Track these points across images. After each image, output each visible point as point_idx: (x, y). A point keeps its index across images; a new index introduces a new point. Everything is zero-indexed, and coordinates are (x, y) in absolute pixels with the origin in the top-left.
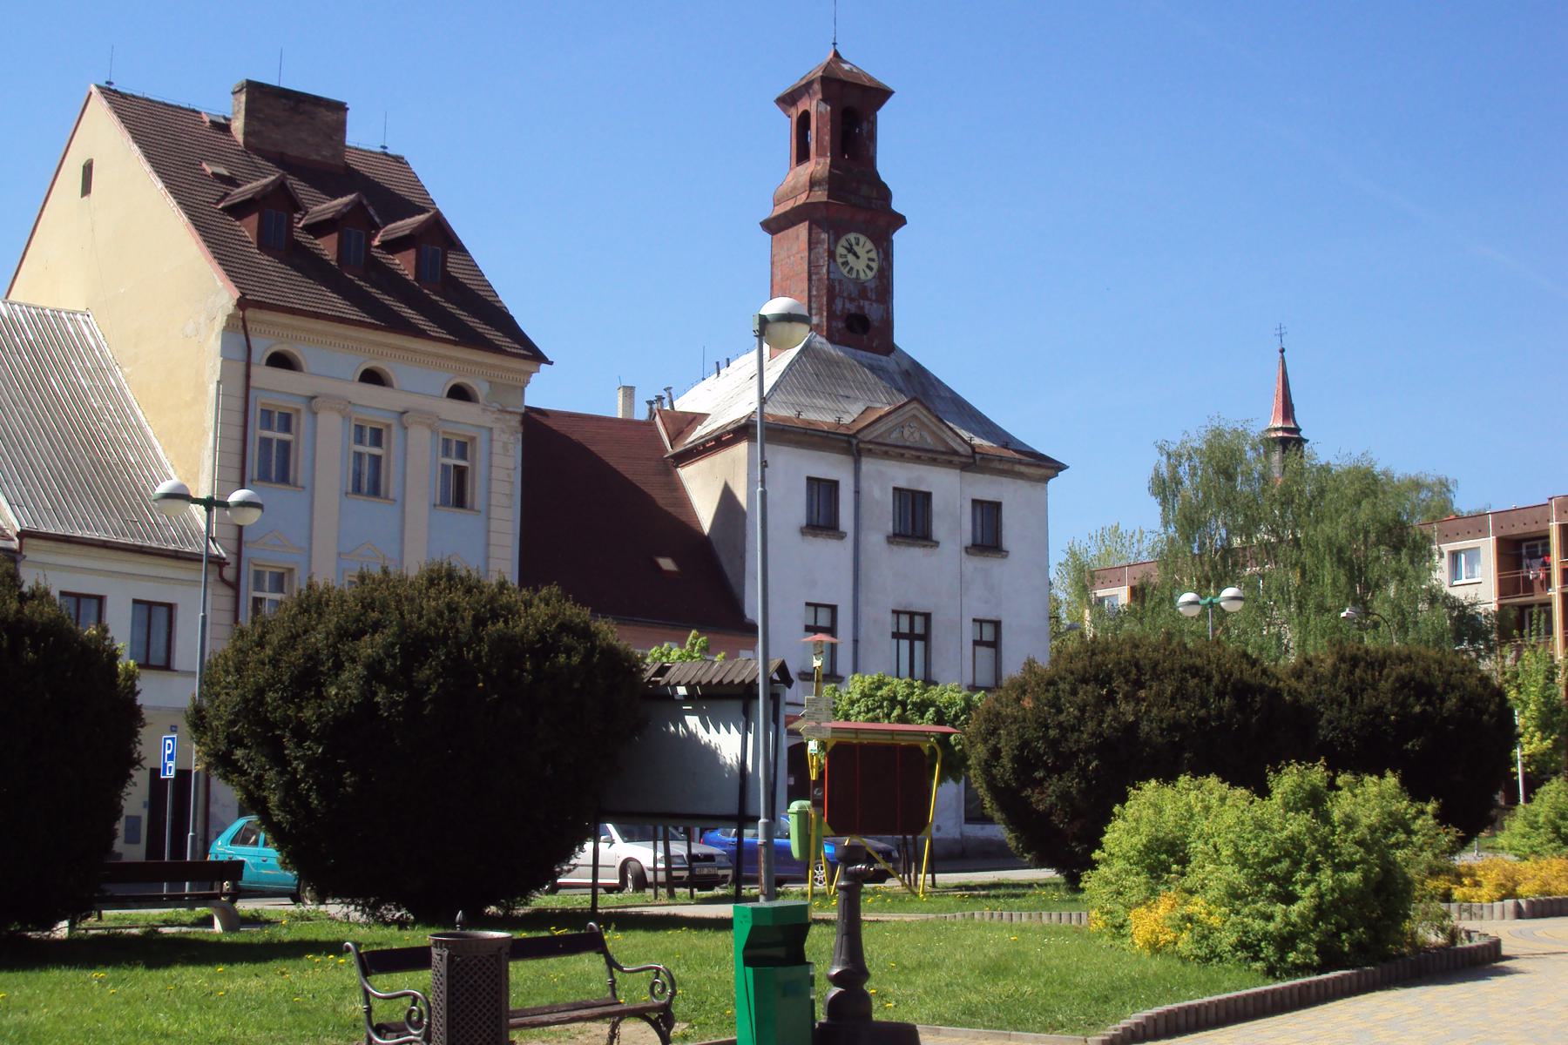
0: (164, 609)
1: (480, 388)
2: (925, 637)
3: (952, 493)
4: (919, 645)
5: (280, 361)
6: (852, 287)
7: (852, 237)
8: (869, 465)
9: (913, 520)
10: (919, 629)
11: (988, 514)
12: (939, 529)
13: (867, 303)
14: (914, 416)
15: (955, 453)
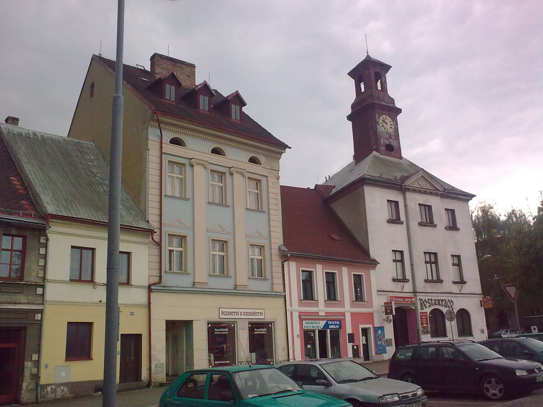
0: (125, 256)
1: (262, 159)
3: (439, 206)
5: (175, 141)
7: (384, 116)
8: (409, 195)
10: (433, 260)
11: (451, 212)
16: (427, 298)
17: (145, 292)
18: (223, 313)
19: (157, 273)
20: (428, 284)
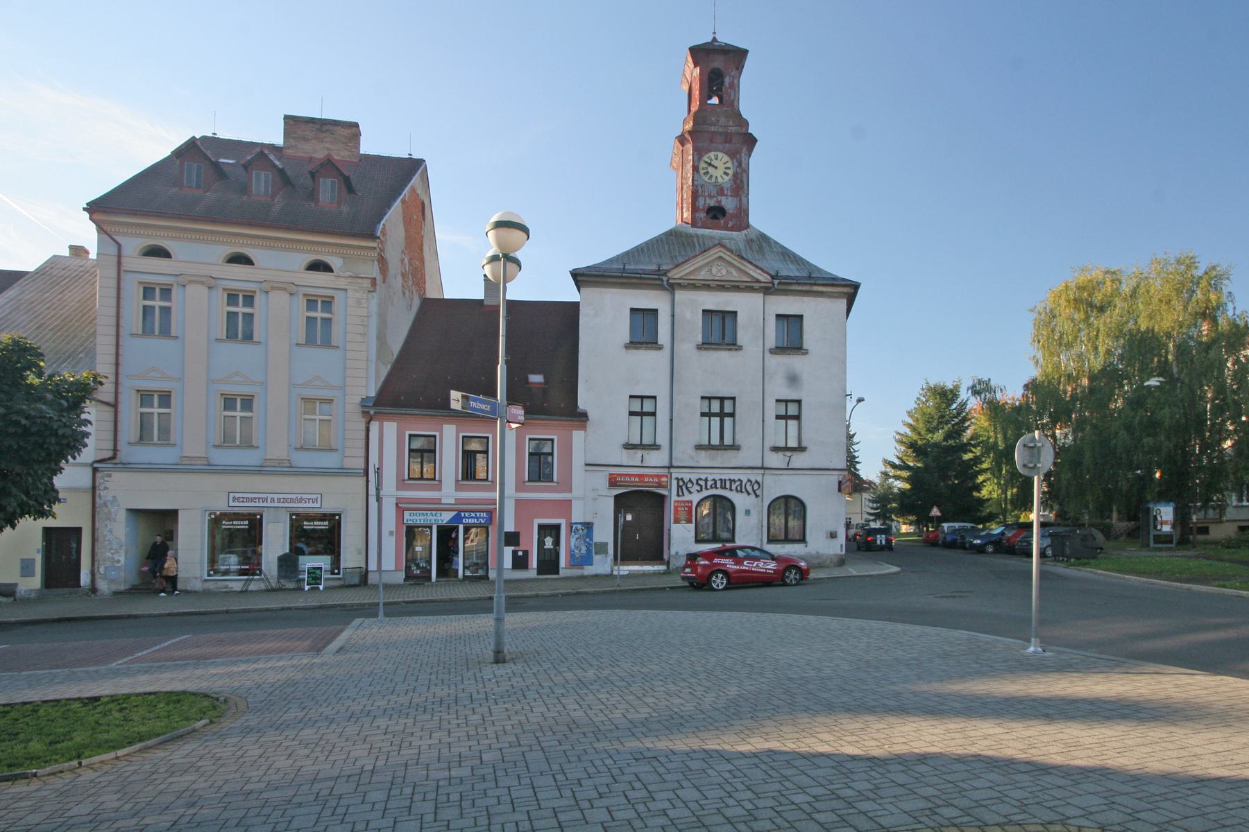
1: (335, 262)
2: (797, 418)
3: (754, 313)
4: (728, 421)
6: (711, 188)
8: (680, 295)
9: (720, 331)
11: (791, 323)
12: (743, 336)
13: (723, 199)
14: (720, 257)
15: (758, 281)
16: (694, 478)
17: (89, 471)
18: (235, 499)
19: (110, 445)
20: (703, 453)
